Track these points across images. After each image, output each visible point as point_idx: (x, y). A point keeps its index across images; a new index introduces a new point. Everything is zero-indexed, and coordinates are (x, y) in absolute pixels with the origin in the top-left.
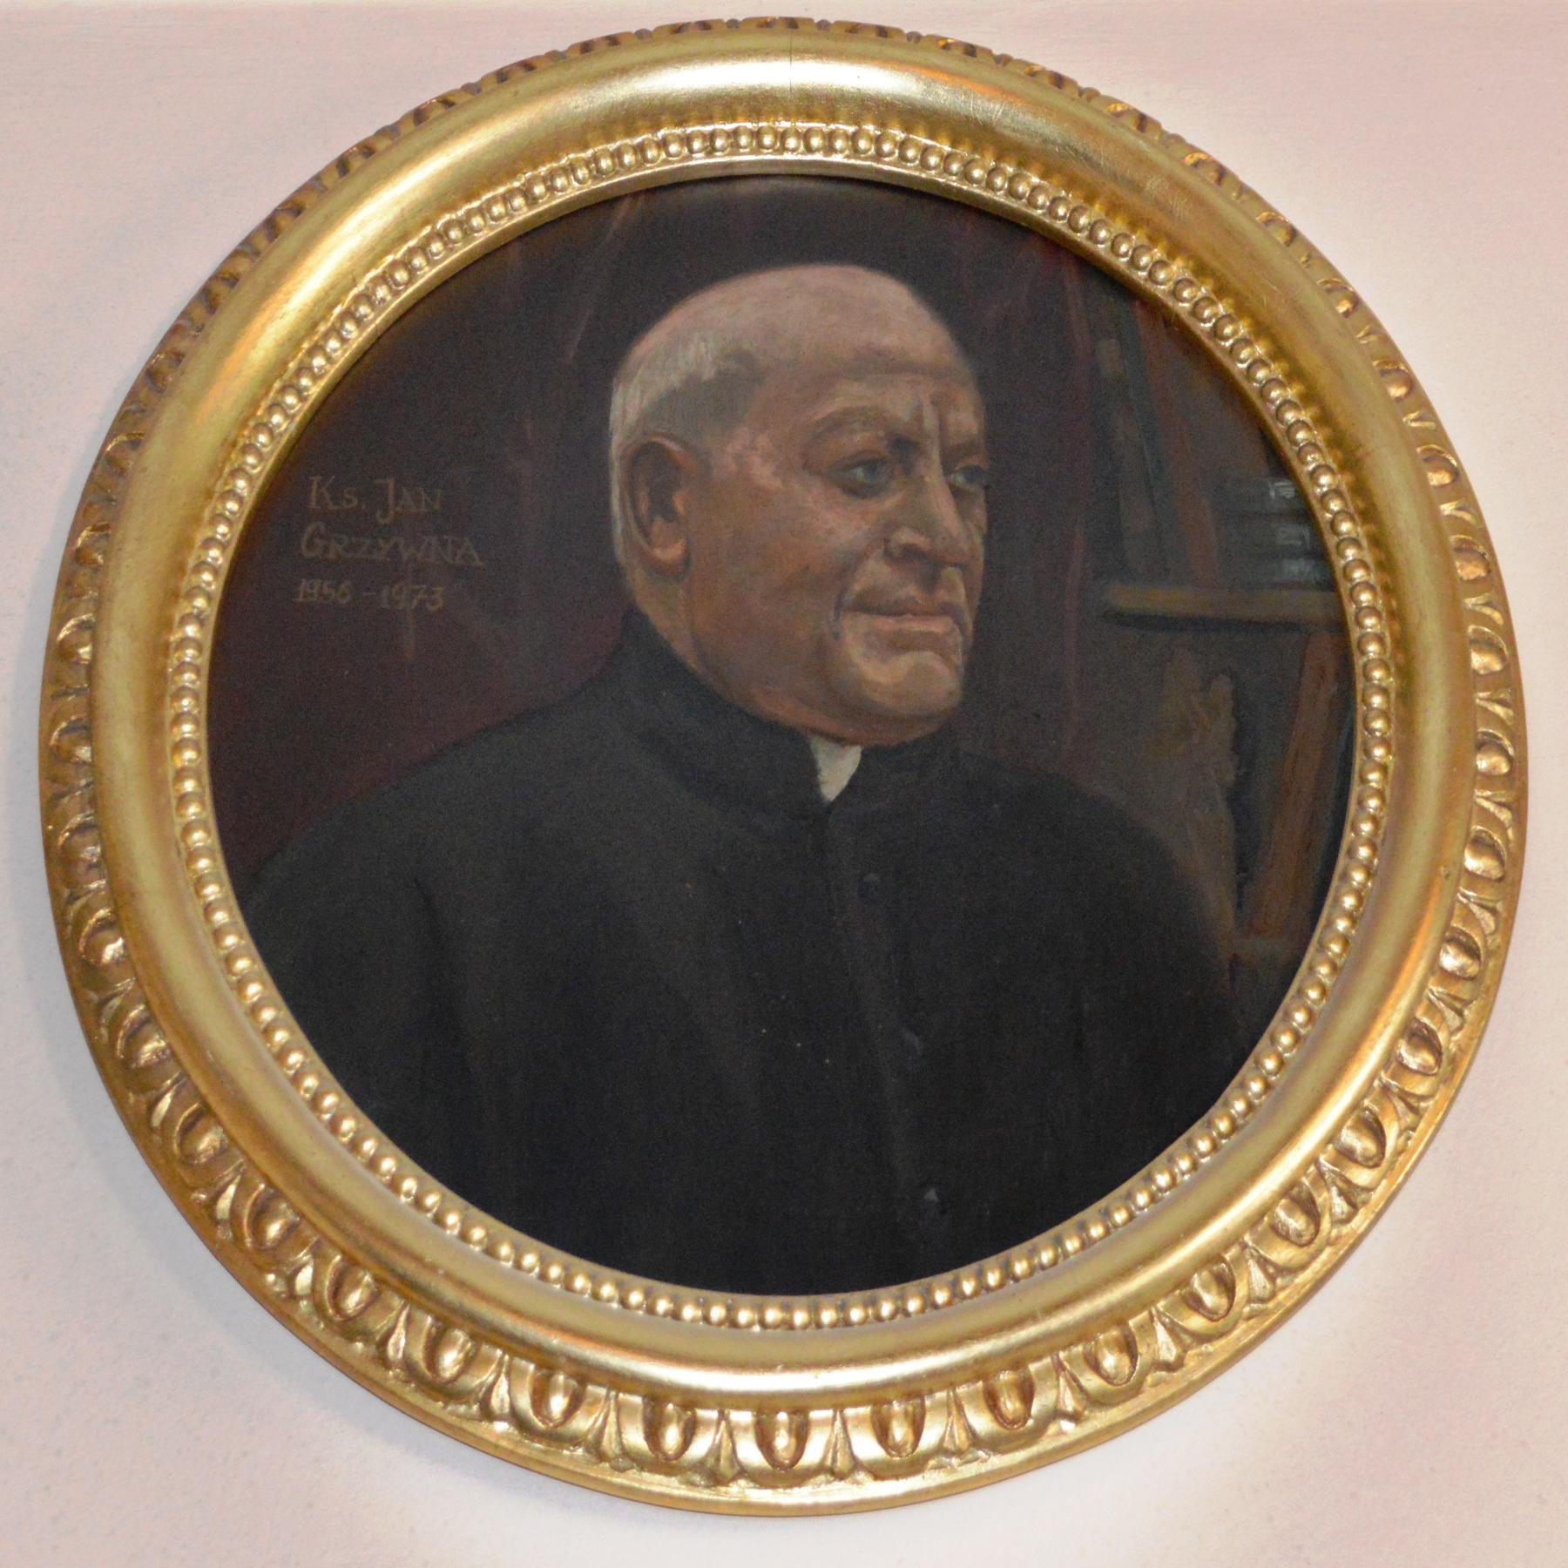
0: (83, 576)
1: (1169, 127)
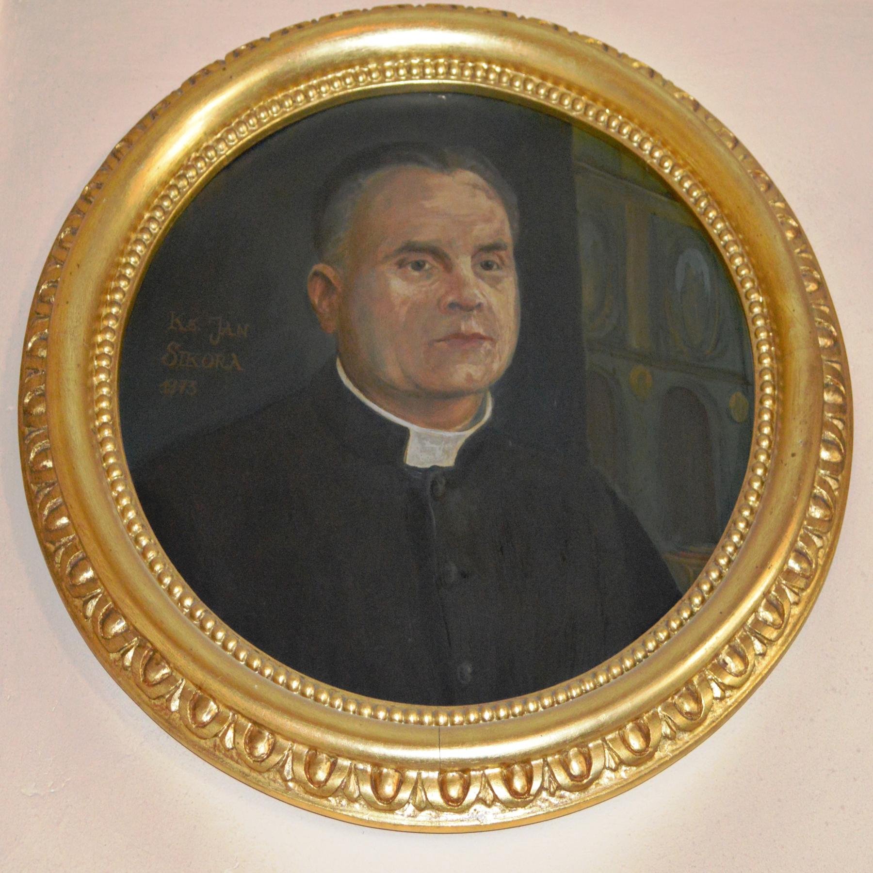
0: (44, 309)
1: (666, 76)
